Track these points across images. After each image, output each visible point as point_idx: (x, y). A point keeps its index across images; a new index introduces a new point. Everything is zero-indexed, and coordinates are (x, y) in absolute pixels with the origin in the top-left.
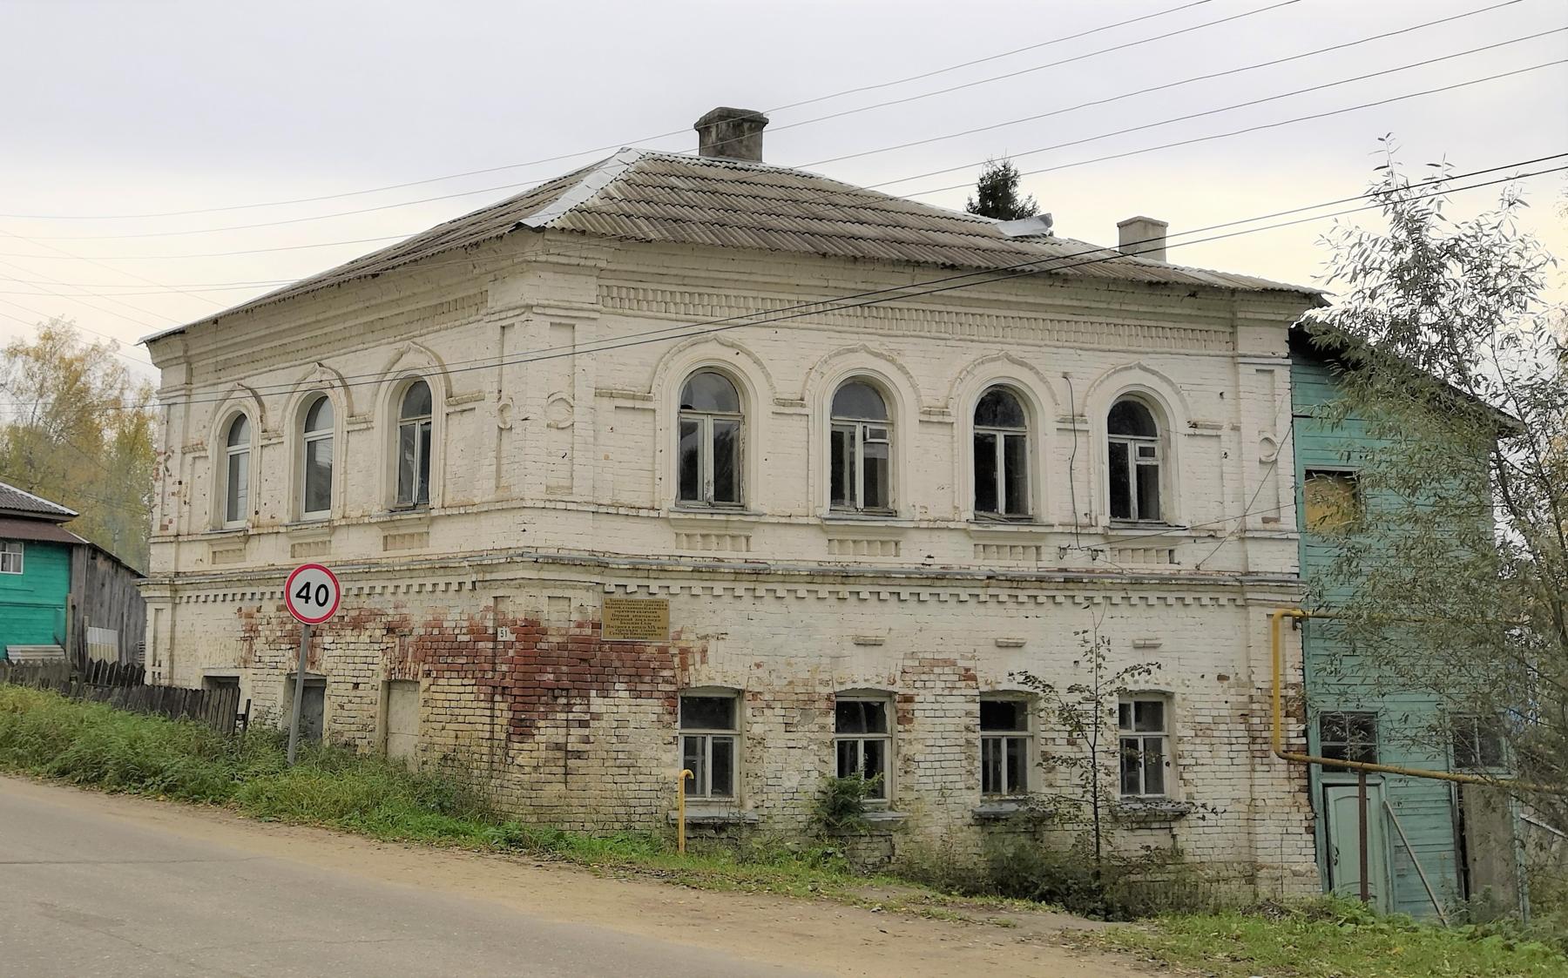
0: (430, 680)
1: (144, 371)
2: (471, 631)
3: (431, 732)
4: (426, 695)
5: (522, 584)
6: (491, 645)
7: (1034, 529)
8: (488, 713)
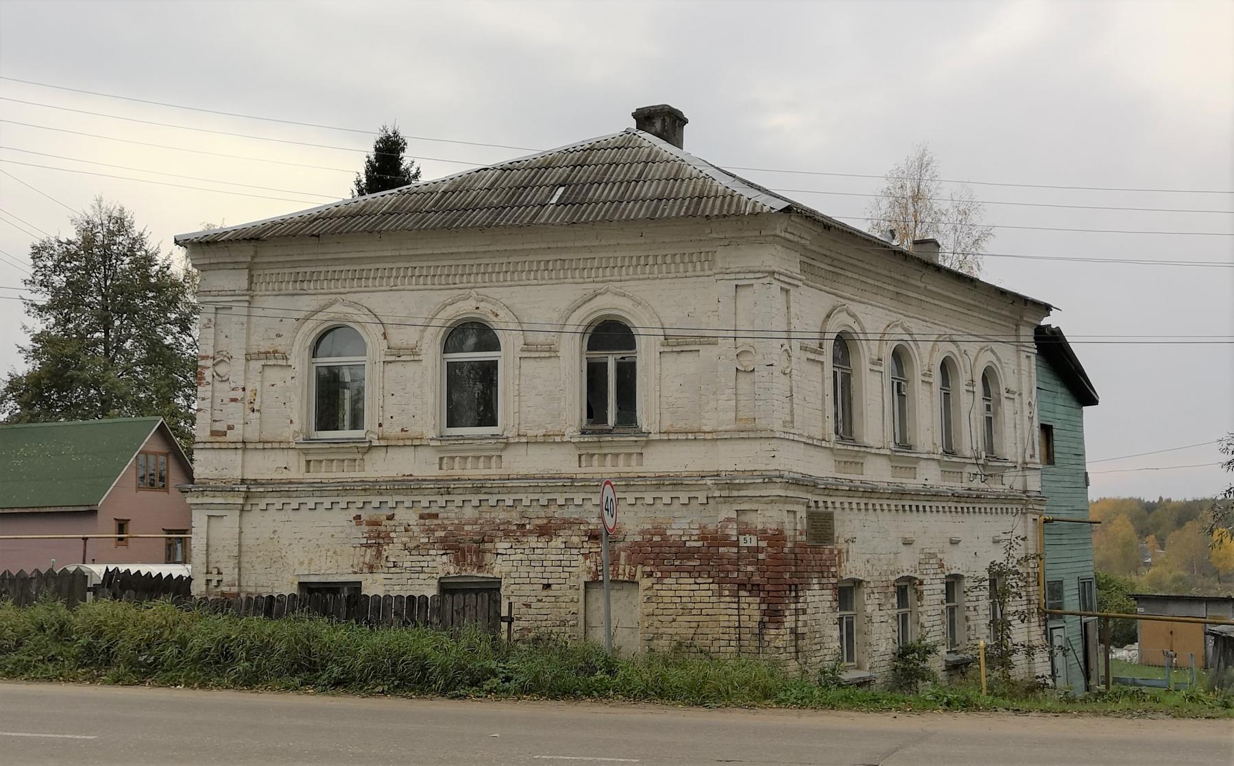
0: (653, 580)
1: (178, 263)
2: (703, 538)
3: (657, 624)
4: (649, 593)
5: (773, 501)
6: (735, 550)
7: (954, 459)
8: (735, 606)
